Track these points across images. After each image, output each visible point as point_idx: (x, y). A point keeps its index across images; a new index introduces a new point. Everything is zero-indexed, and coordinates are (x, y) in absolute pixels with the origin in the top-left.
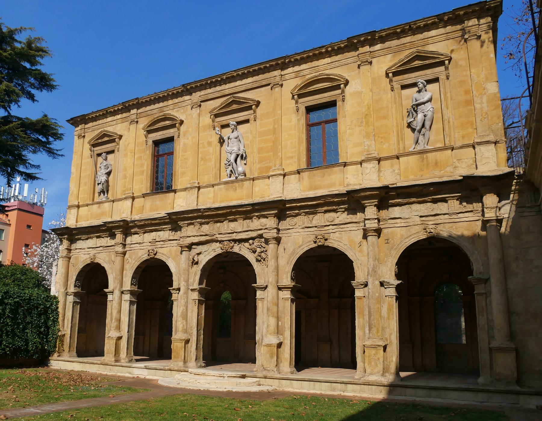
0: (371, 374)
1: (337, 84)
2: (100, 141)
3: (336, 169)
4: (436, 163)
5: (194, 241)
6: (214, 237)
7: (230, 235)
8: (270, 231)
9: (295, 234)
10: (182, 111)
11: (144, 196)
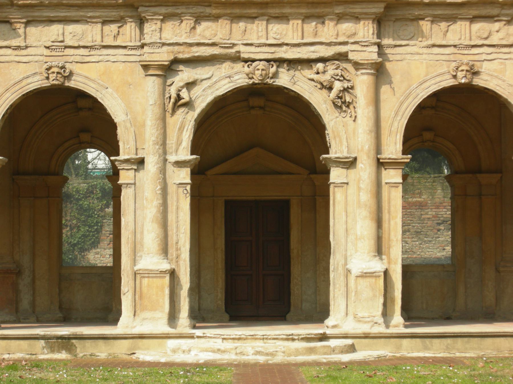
5: (181, 56)
6: (233, 51)
7: (273, 49)
8: (365, 49)
9: (408, 57)
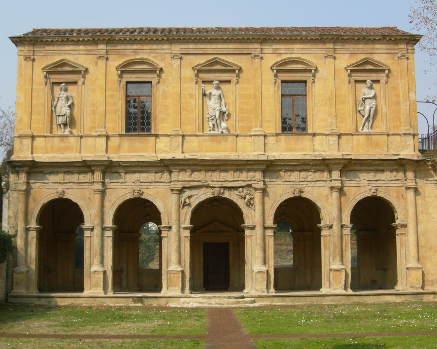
1: (312, 70)
2: (60, 69)
3: (307, 137)
7: (222, 183)
10: (160, 58)
11: (120, 136)
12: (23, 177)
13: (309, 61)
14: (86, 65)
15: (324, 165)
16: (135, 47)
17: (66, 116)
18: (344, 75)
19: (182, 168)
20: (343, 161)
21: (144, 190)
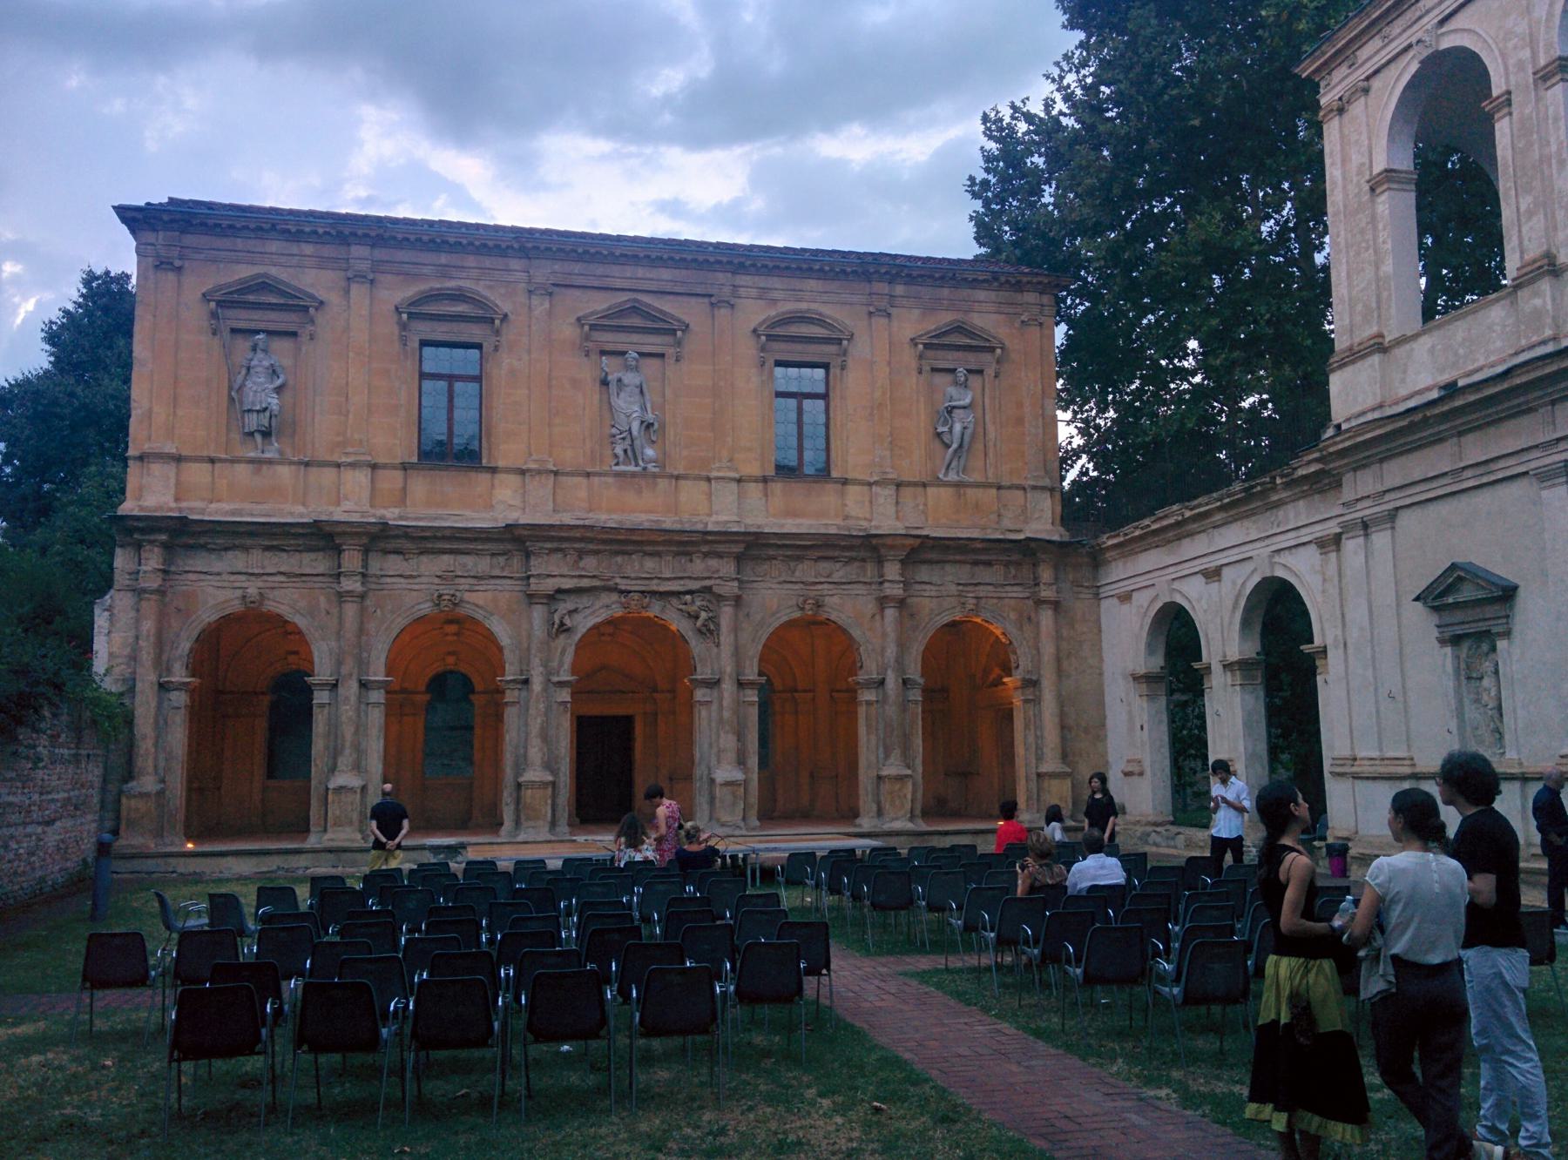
0: (893, 819)
2: (251, 298)
3: (830, 487)
4: (977, 506)
11: (405, 467)
12: (153, 560)
13: (836, 320)
14: (321, 294)
15: (866, 548)
16: (444, 259)
17: (267, 414)
18: (908, 357)
19: (555, 545)
20: (910, 541)
21: (467, 596)
